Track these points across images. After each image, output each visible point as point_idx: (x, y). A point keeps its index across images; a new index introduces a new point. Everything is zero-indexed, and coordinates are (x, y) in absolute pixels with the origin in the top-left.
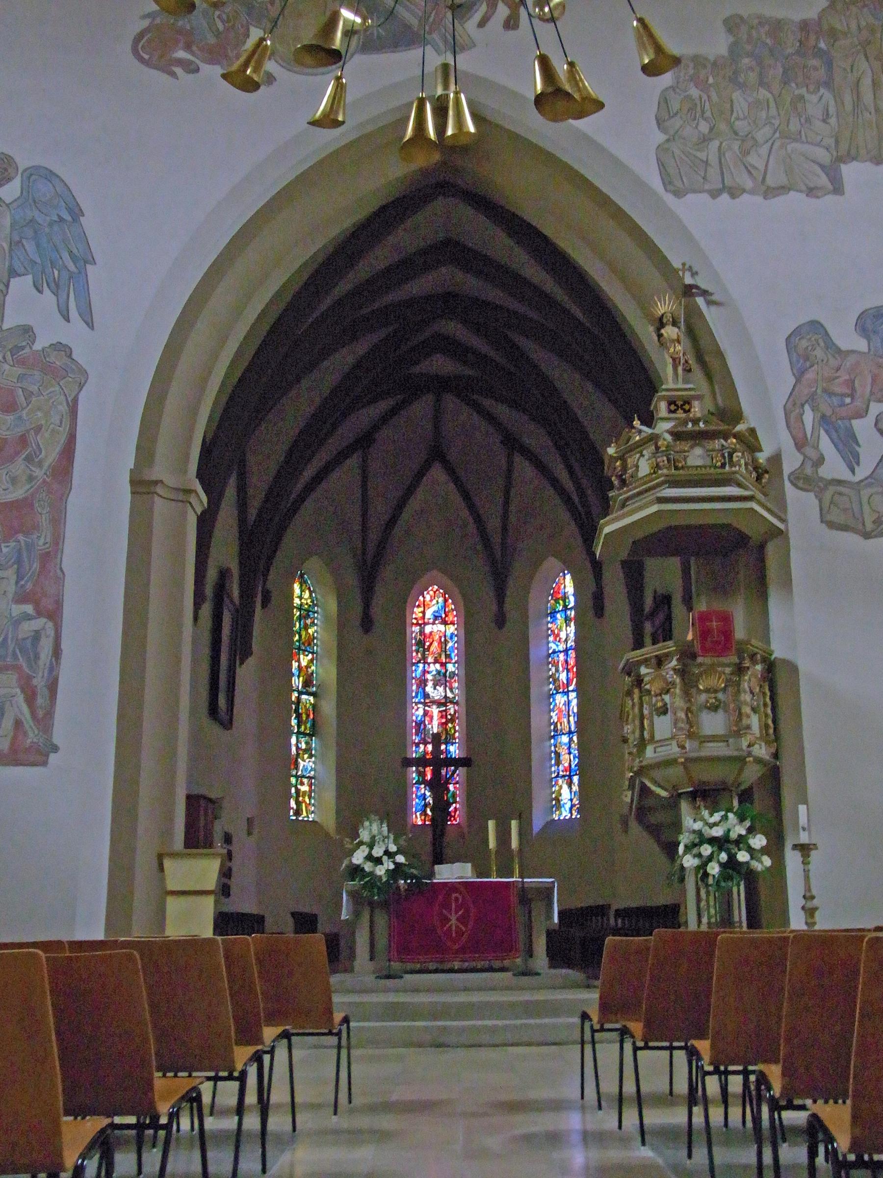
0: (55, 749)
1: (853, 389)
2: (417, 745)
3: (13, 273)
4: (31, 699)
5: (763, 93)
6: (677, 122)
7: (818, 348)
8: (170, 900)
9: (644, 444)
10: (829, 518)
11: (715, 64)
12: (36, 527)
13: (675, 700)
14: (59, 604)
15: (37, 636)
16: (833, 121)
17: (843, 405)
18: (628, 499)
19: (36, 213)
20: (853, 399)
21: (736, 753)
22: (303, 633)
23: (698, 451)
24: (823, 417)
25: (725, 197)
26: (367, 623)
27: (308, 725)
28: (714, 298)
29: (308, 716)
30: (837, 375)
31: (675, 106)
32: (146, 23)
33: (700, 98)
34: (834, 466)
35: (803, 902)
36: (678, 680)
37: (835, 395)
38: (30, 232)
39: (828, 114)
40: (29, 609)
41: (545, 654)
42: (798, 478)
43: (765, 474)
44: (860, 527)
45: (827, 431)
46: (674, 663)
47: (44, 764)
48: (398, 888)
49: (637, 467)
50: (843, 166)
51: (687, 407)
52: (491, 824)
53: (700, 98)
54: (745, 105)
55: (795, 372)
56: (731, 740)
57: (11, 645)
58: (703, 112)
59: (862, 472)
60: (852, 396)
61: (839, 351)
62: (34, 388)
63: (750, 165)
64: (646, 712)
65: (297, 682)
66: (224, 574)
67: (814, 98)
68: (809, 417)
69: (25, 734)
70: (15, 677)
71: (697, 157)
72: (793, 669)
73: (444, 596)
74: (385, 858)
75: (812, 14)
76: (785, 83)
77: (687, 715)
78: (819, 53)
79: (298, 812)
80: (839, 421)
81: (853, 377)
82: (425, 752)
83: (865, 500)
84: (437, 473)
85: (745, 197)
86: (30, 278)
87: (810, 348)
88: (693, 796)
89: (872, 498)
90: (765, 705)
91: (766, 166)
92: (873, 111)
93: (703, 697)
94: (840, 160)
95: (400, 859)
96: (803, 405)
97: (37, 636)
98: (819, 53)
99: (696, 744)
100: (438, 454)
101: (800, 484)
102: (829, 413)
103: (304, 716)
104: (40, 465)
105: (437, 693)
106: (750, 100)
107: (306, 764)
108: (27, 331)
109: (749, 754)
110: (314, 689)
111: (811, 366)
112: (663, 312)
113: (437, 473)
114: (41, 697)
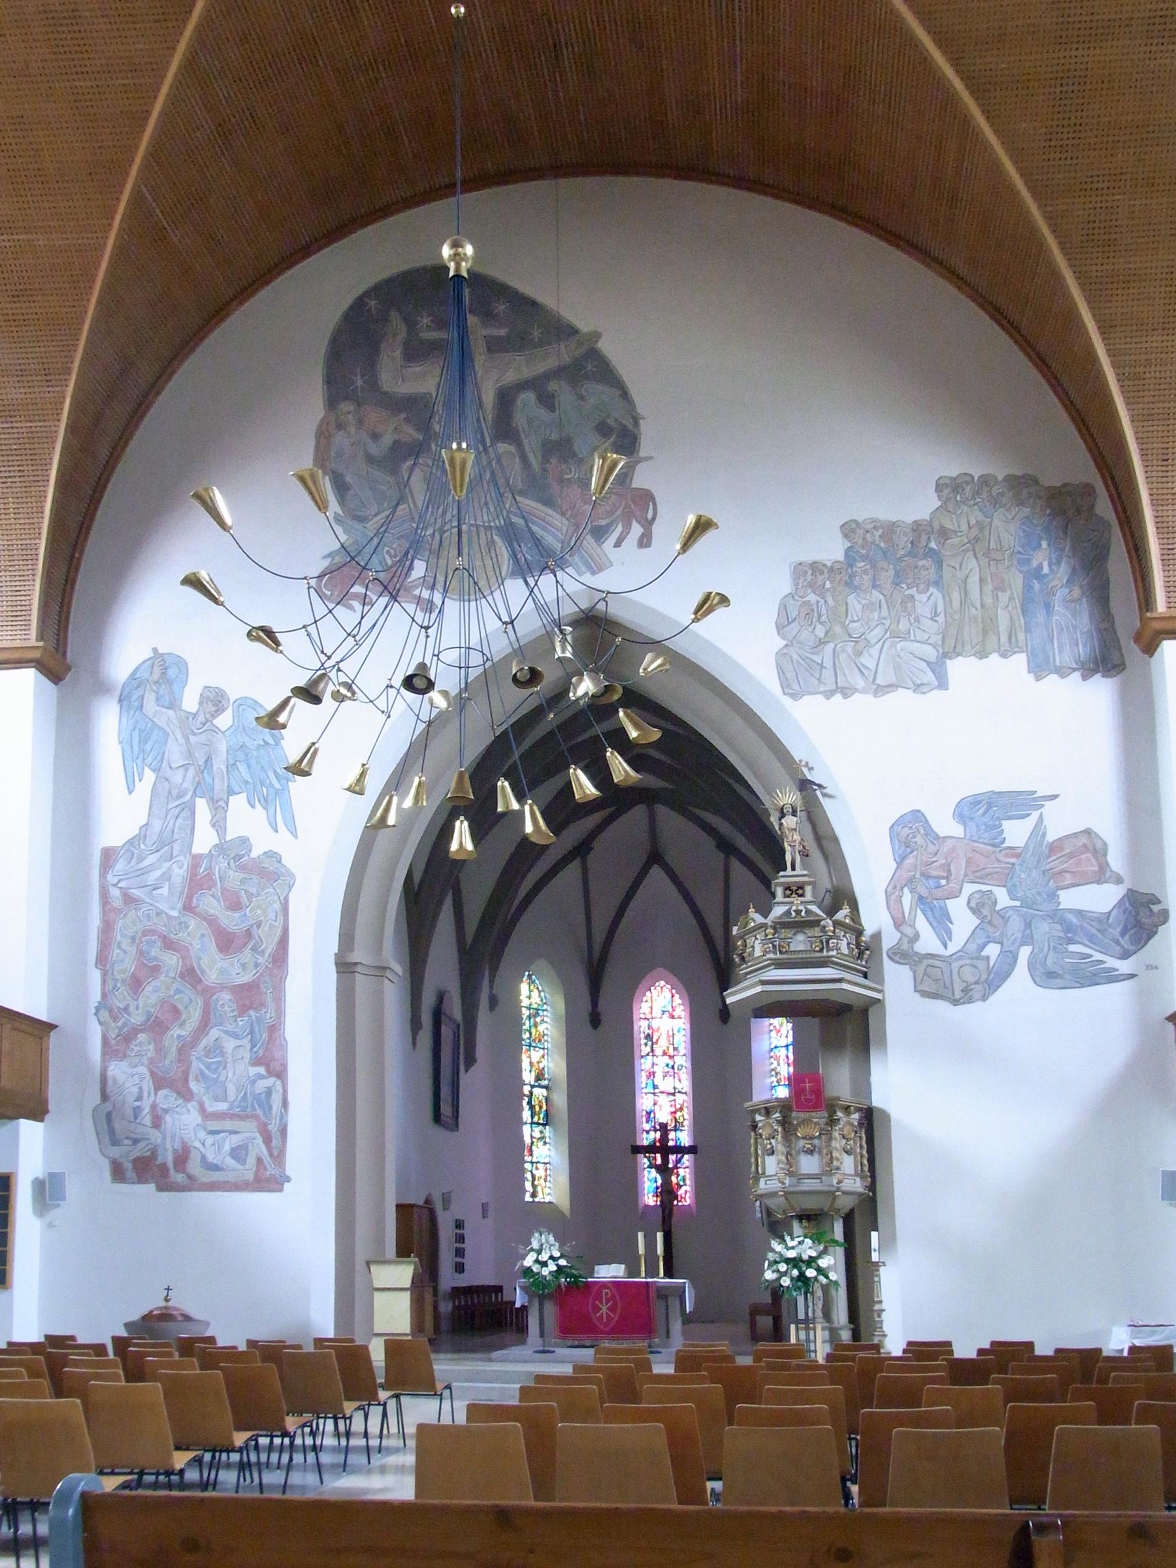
0: (288, 1179)
1: (949, 871)
2: (648, 1132)
3: (231, 792)
4: (268, 1140)
5: (876, 595)
6: (795, 627)
8: (376, 1294)
11: (831, 570)
12: (262, 1005)
13: (778, 1144)
14: (284, 1067)
15: (269, 1092)
16: (941, 618)
18: (747, 974)
19: (246, 739)
21: (826, 1189)
22: (533, 1030)
23: (800, 937)
24: (921, 898)
25: (838, 696)
26: (595, 1020)
27: (542, 1116)
29: (541, 1107)
31: (793, 613)
32: (327, 562)
33: (818, 602)
34: (929, 942)
38: (241, 756)
40: (262, 1070)
41: (768, 1048)
42: (895, 954)
43: (865, 952)
46: (778, 1115)
47: (281, 1190)
48: (560, 1286)
51: (800, 892)
52: (640, 1235)
53: (818, 602)
54: (859, 607)
57: (250, 1099)
58: (820, 616)
59: (954, 947)
60: (947, 878)
61: (937, 837)
62: (254, 890)
63: (864, 665)
65: (528, 1077)
66: (441, 997)
67: (923, 598)
69: (265, 1169)
70: (255, 1124)
72: (886, 1116)
73: (671, 991)
74: (550, 1261)
75: (925, 515)
76: (897, 584)
78: (930, 553)
79: (534, 1195)
82: (654, 1141)
83: (955, 971)
84: (656, 873)
86: (244, 795)
88: (800, 1218)
90: (861, 1147)
92: (979, 607)
93: (802, 1143)
94: (945, 655)
95: (563, 1262)
97: (269, 1092)
98: (930, 553)
99: (795, 1180)
100: (655, 857)
101: (897, 958)
102: (925, 894)
103: (537, 1108)
104: (262, 953)
105: (666, 1085)
107: (541, 1152)
108: (244, 841)
109: (838, 1189)
110: (546, 1082)
113: (656, 873)
114: (275, 1139)
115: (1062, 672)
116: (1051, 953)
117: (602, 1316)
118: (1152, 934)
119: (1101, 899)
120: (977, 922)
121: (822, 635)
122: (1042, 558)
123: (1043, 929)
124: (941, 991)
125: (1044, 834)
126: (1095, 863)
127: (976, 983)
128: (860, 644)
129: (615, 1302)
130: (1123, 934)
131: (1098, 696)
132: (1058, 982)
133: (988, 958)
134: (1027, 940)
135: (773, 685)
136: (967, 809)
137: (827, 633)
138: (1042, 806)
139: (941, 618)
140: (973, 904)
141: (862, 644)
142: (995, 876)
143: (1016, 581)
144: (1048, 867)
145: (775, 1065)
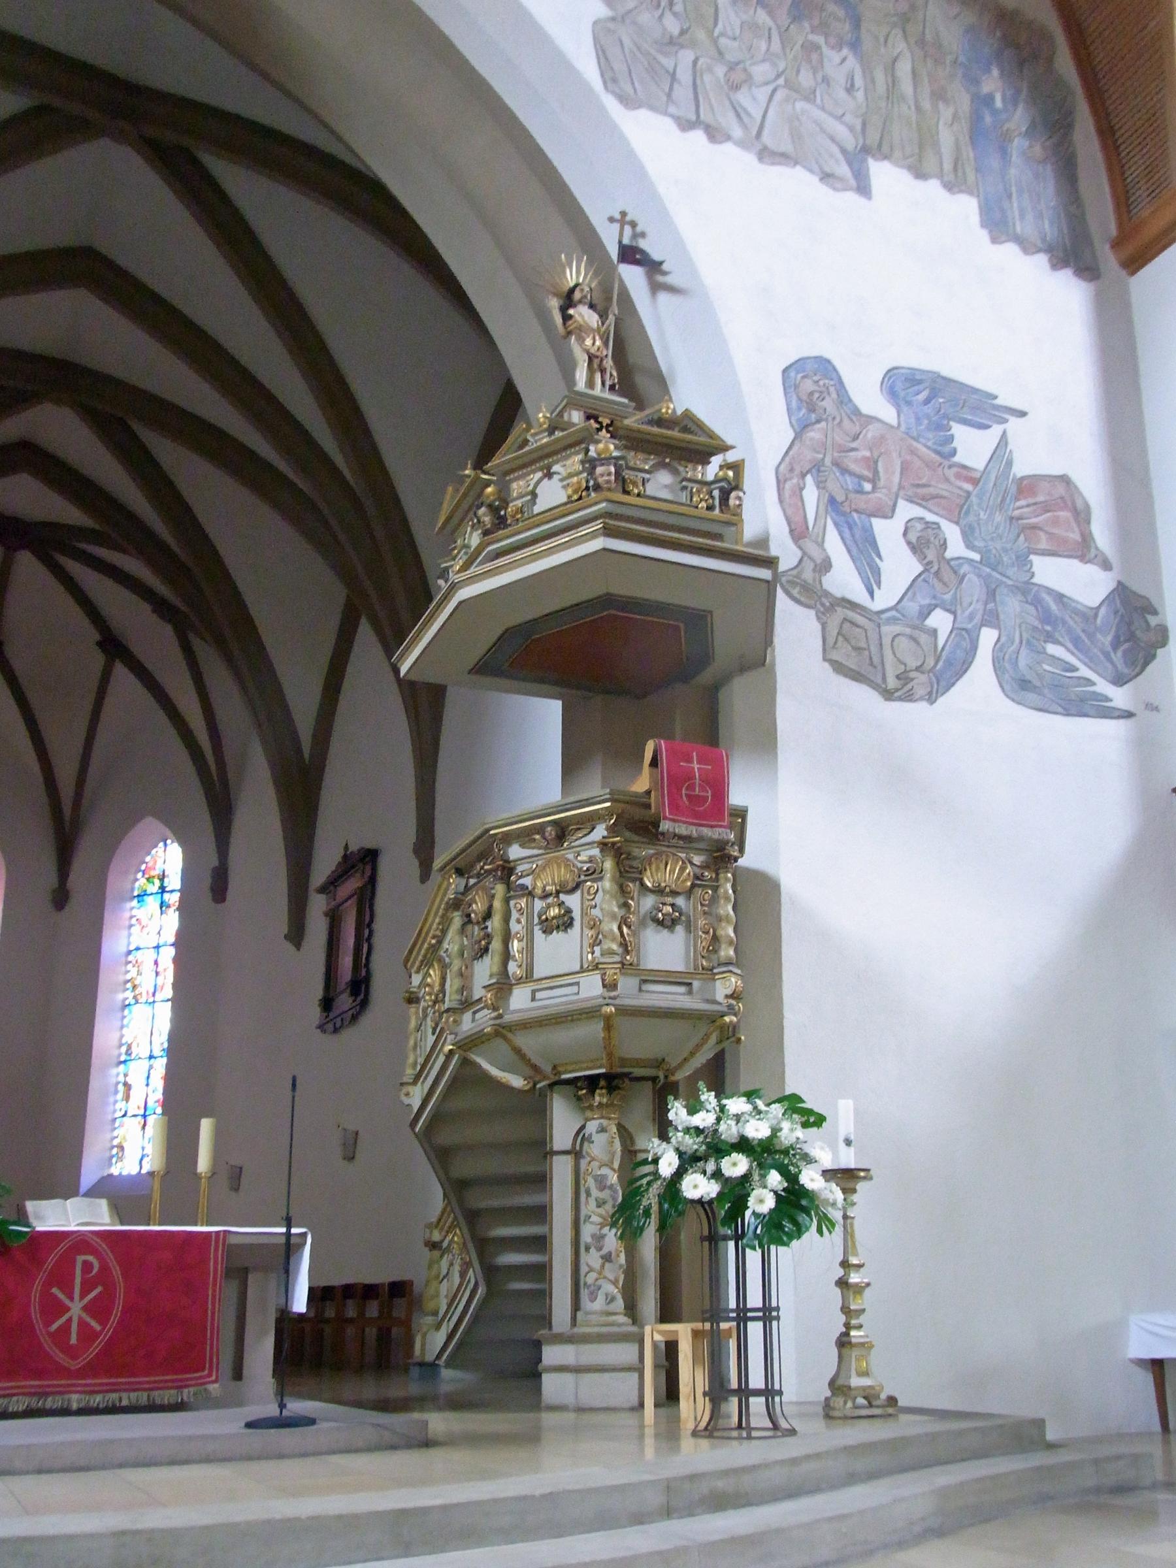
1: (876, 472)
7: (827, 398)
9: (556, 453)
10: (835, 656)
13: (603, 897)
17: (860, 491)
20: (874, 488)
24: (832, 501)
28: (668, 279)
30: (854, 445)
34: (844, 578)
35: (840, 1272)
36: (608, 865)
37: (852, 474)
39: (852, 85)
41: (124, 949)
44: (879, 680)
45: (836, 524)
49: (534, 495)
50: (871, 161)
55: (794, 422)
56: (696, 984)
59: (884, 599)
61: (857, 412)
63: (741, 106)
64: (514, 927)
67: (836, 57)
68: (811, 495)
71: (659, 63)
77: (620, 928)
80: (855, 515)
81: (876, 455)
83: (887, 641)
85: (728, 147)
87: (816, 395)
89: (897, 640)
91: (764, 116)
93: (649, 902)
94: (866, 150)
96: (803, 476)
102: (840, 498)
106: (745, 17)
111: (818, 421)
112: (572, 284)
115: (1027, 248)
116: (1024, 652)
117: (66, 1329)
118: (1149, 658)
119: (1084, 584)
120: (920, 568)
121: (676, 31)
122: (993, 83)
123: (1012, 606)
124: (866, 670)
125: (1010, 464)
126: (1076, 529)
127: (918, 669)
128: (737, 79)
129: (109, 1288)
130: (1115, 645)
131: (1065, 299)
132: (1031, 697)
133: (934, 632)
134: (991, 619)
135: (589, 68)
136: (902, 384)
137: (683, 32)
138: (1006, 421)
139: (860, 95)
140: (913, 537)
141: (738, 76)
142: (943, 501)
143: (964, 102)
144: (1017, 513)
145: (133, 973)
